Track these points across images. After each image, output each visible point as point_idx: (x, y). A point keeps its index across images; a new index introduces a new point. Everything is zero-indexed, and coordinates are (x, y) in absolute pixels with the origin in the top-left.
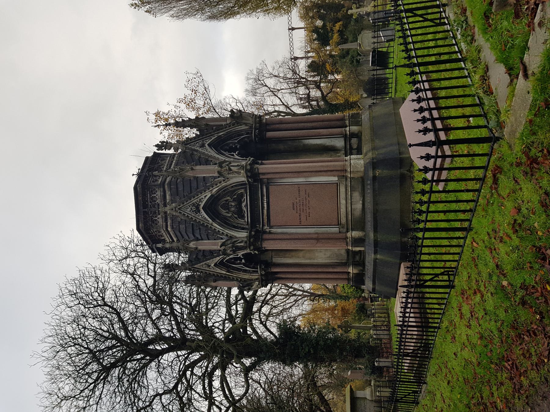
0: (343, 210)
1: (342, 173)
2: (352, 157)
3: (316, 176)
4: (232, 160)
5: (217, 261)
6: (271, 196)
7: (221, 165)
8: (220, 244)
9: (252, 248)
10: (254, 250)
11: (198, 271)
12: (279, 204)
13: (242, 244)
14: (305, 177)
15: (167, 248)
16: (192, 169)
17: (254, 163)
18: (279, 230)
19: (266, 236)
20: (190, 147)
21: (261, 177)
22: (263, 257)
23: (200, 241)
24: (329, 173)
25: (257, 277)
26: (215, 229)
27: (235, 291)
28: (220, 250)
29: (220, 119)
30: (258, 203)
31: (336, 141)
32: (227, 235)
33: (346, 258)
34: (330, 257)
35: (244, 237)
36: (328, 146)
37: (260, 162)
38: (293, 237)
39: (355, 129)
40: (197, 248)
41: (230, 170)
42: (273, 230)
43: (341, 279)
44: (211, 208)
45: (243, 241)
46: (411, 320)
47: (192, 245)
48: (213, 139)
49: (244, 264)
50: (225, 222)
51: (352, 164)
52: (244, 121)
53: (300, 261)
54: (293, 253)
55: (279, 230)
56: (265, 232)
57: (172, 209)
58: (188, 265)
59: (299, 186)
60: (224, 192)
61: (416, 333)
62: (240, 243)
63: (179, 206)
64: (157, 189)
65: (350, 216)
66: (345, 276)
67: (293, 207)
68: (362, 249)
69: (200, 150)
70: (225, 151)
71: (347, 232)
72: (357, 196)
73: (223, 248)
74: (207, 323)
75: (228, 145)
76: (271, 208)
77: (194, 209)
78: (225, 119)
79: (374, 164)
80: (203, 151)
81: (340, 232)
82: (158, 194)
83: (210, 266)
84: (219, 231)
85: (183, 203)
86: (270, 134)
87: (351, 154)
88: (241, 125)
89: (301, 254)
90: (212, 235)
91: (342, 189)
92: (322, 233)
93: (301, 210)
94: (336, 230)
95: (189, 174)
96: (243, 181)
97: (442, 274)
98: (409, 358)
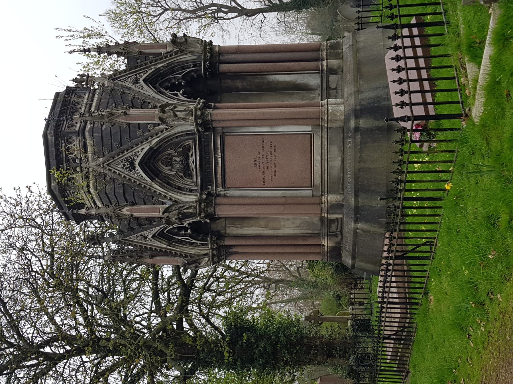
0: (317, 168)
1: (316, 121)
2: (330, 100)
3: (283, 125)
4: (176, 102)
5: (156, 231)
6: (226, 150)
7: (163, 108)
8: (162, 210)
9: (203, 215)
10: (206, 217)
11: (130, 245)
12: (237, 160)
13: (190, 210)
14: (271, 126)
15: (92, 215)
16: (125, 114)
17: (206, 106)
18: (237, 193)
19: (219, 200)
20: (120, 83)
21: (215, 125)
22: (215, 227)
23: (136, 207)
24: (301, 121)
25: (206, 252)
26: (155, 191)
27: (167, 271)
28: (161, 218)
29: (157, 43)
30: (210, 158)
31: (310, 78)
32: (171, 199)
33: (319, 227)
34: (299, 227)
35: (193, 202)
36: (299, 84)
37: (213, 104)
38: (254, 201)
39: (334, 62)
40: (132, 215)
41: (176, 116)
42: (229, 193)
43: (314, 253)
44: (149, 164)
45: (191, 206)
46: (393, 290)
47: (126, 211)
48: (150, 72)
49: (190, 235)
50: (167, 182)
51: (330, 111)
52: (190, 49)
53: (261, 232)
54: (253, 222)
55: (237, 193)
56: (218, 196)
57: (99, 165)
58: (118, 237)
59: (263, 137)
60: (166, 143)
61: (399, 311)
62: (187, 208)
63: (108, 161)
64: (74, 138)
65: (326, 176)
66: (318, 250)
67: (255, 164)
68: (340, 216)
69: (133, 87)
70: (166, 89)
71: (322, 196)
72: (335, 150)
73: (166, 215)
74: (125, 316)
75: (169, 80)
76: (227, 164)
77: (127, 165)
78: (164, 46)
79: (359, 112)
80: (137, 89)
81: (313, 196)
82: (76, 144)
83: (146, 238)
84: (160, 194)
85: (113, 158)
86: (224, 67)
87: (329, 96)
88: (186, 54)
89: (262, 223)
90: (150, 198)
91: (317, 142)
92: (291, 197)
93: (266, 168)
94: (308, 193)
95: (121, 120)
96: (191, 130)
97: (425, 244)
98: (392, 342)
